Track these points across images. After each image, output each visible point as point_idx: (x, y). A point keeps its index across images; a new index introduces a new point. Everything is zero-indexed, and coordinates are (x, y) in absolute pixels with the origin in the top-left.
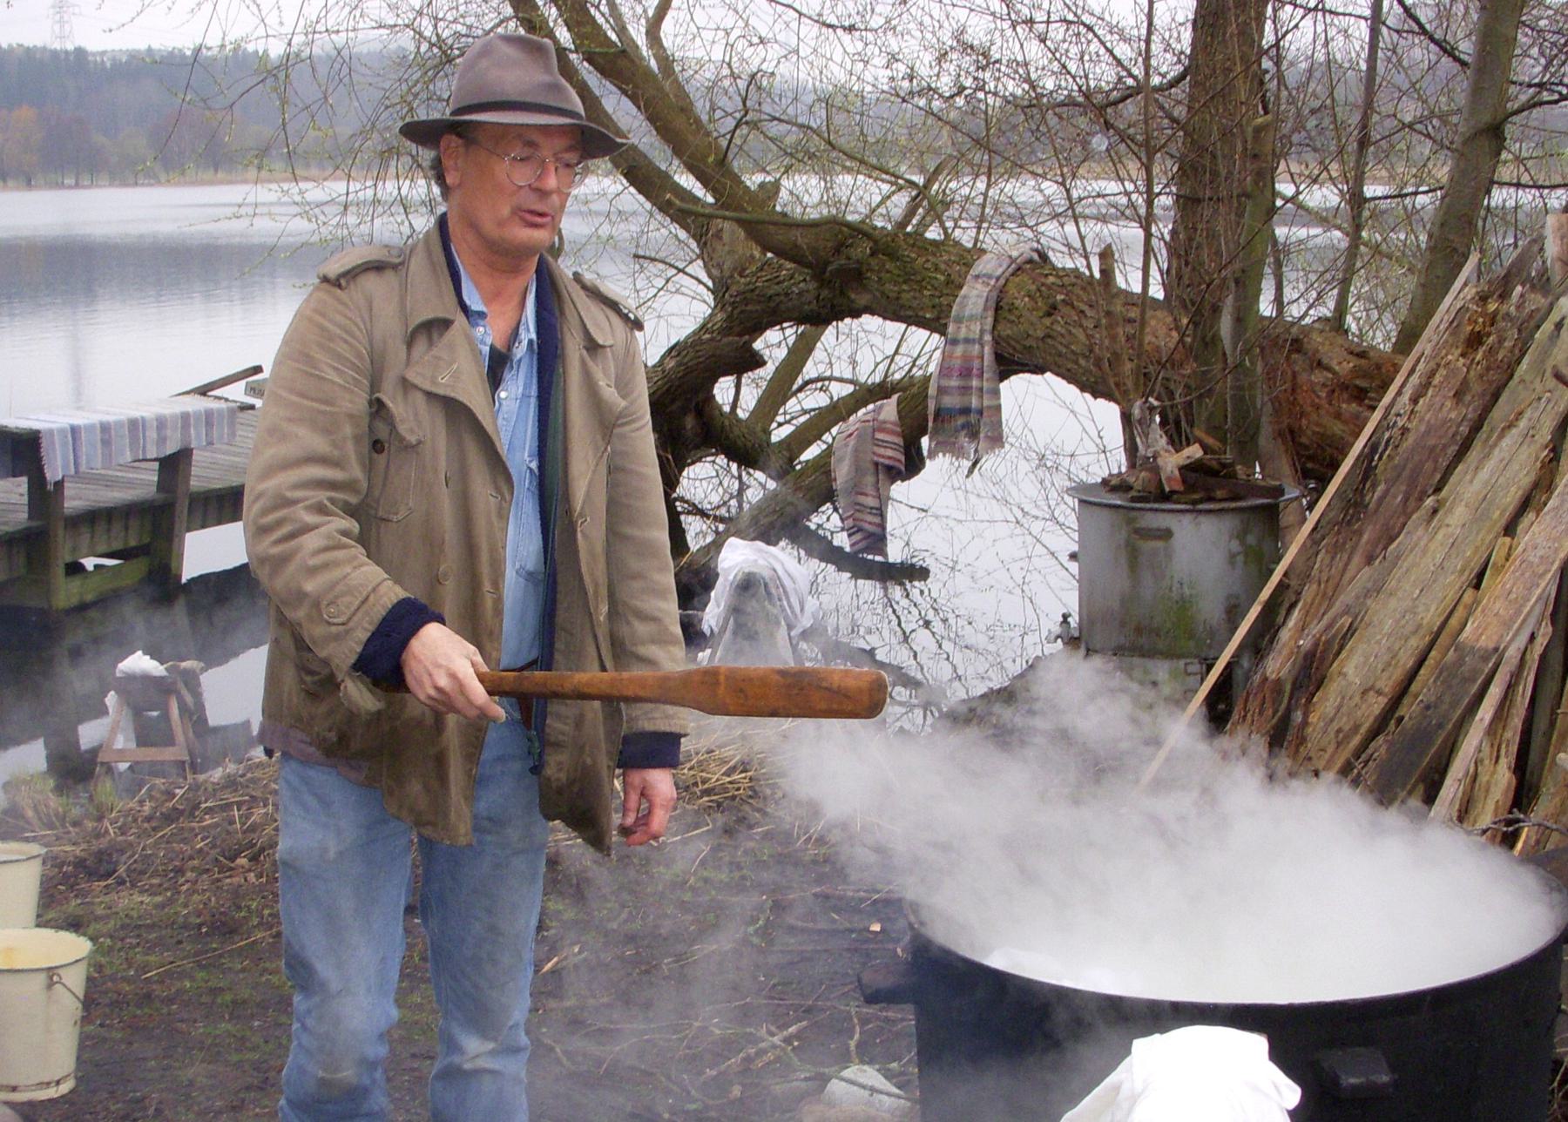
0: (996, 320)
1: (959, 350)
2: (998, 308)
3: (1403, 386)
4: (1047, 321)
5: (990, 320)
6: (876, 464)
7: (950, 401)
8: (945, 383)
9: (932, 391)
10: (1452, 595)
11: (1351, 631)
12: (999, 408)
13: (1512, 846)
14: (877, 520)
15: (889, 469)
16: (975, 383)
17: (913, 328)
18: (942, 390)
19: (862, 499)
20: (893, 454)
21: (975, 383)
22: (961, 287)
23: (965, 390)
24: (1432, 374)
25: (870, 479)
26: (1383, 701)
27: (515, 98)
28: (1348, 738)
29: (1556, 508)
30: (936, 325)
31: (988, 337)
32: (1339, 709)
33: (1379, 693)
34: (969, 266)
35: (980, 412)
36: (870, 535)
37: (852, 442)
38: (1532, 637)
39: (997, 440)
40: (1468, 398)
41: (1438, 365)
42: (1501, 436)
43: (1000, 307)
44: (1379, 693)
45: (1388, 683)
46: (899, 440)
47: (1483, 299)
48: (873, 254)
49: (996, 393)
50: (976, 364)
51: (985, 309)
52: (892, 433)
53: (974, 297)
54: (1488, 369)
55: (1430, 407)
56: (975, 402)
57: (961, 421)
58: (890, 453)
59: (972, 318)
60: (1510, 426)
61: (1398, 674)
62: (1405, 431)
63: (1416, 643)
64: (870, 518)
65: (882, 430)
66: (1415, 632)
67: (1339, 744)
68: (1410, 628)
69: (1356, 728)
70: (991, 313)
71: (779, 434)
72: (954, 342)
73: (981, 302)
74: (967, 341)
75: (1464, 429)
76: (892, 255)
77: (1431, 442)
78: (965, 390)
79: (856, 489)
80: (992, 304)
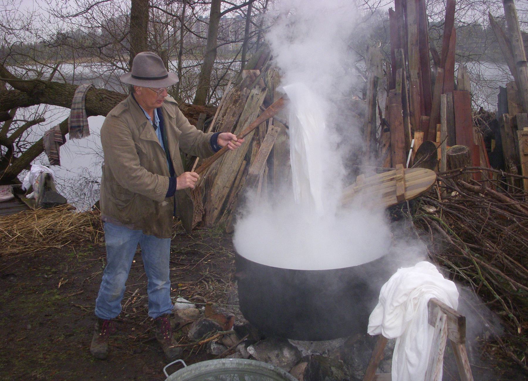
0: (85, 103)
1: (76, 111)
2: (86, 100)
3: (219, 113)
4: (101, 102)
5: (84, 103)
6: (55, 142)
7: (74, 124)
8: (72, 120)
9: (69, 122)
10: (240, 162)
11: (216, 174)
12: (88, 125)
13: (145, 275)
14: (57, 156)
15: (59, 142)
16: (81, 119)
17: (52, 107)
18: (72, 122)
19: (52, 151)
20: (60, 139)
21: (81, 119)
22: (74, 95)
23: (79, 121)
24: (227, 110)
25: (54, 146)
26: (228, 189)
27: (156, 76)
28: (222, 199)
29: (266, 140)
30: (67, 104)
31: (84, 108)
32: (218, 192)
33: (227, 187)
34: (75, 90)
35: (83, 127)
36: (55, 160)
37: (48, 137)
38: (265, 171)
39: (88, 133)
40: (235, 115)
41: (228, 108)
42: (244, 124)
43: (86, 99)
44: (227, 187)
45: (228, 185)
46: (61, 135)
47: (237, 91)
48: (46, 88)
49: (87, 121)
50: (81, 114)
51: (82, 100)
52: (59, 133)
53: (78, 96)
54: (240, 108)
55: (227, 118)
56: (82, 124)
57: (78, 129)
58: (59, 139)
59: (78, 103)
60: (246, 121)
61: (231, 182)
62: (221, 124)
63: (233, 175)
64: (55, 156)
65: (56, 133)
66: (233, 172)
67: (220, 201)
68: (231, 171)
69: (223, 196)
70: (84, 101)
71: (9, 135)
72: (74, 109)
73: (81, 98)
74: (78, 109)
75: (235, 123)
76: (51, 88)
77: (228, 126)
78: (79, 121)
79: (51, 148)
80: (84, 99)
